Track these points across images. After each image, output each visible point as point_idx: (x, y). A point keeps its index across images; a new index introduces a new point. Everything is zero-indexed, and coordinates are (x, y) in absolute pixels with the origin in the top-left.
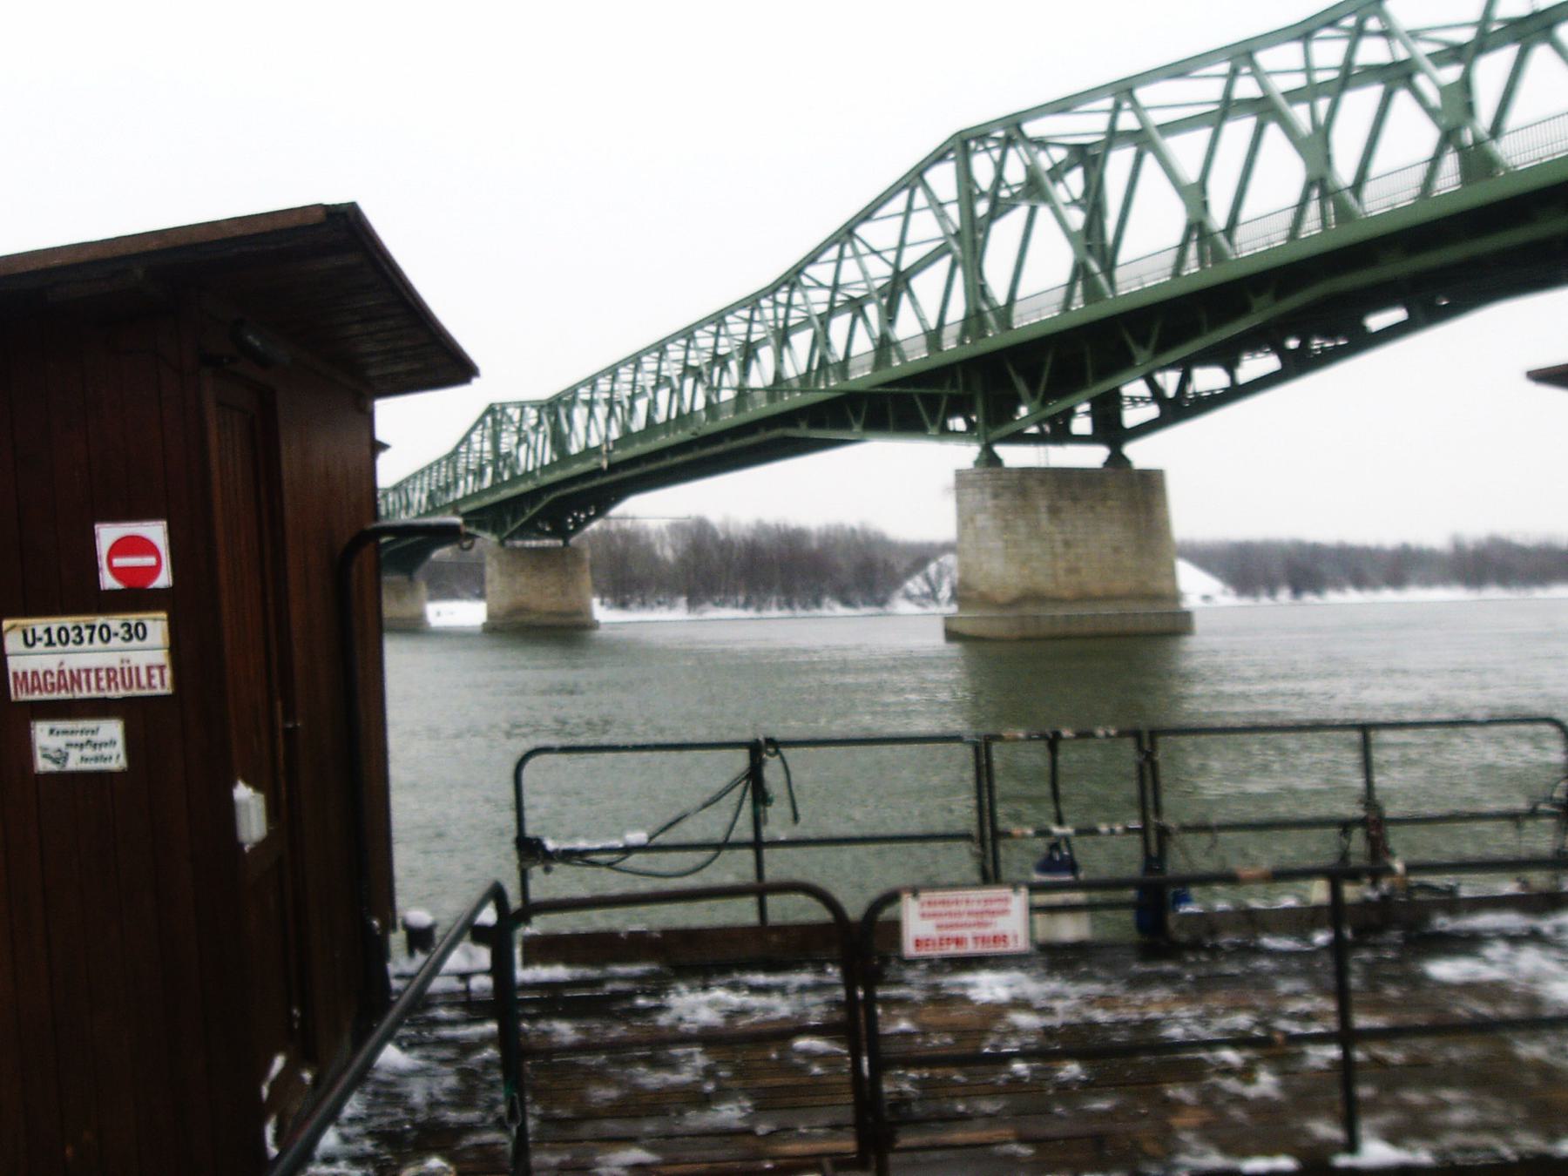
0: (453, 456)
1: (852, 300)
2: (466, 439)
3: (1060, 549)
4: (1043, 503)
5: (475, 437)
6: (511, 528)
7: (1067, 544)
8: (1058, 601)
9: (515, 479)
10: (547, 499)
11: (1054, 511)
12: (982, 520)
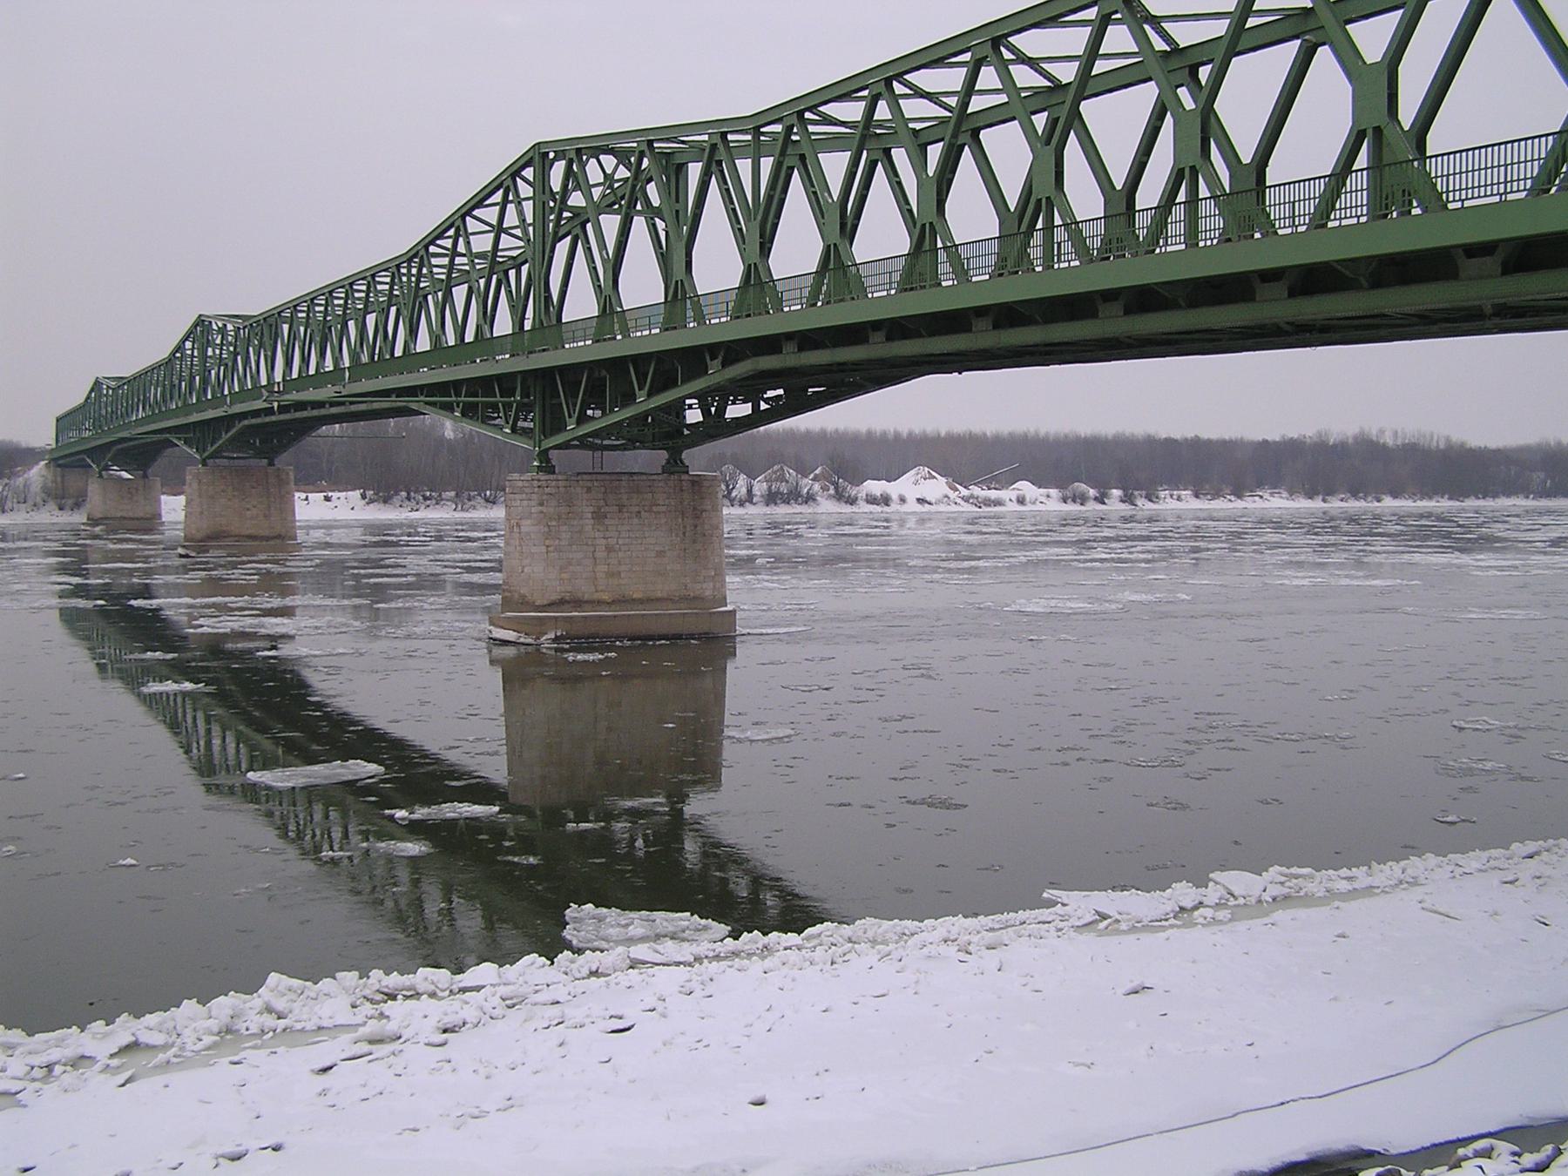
0: (420, 254)
1: (1176, 51)
2: (180, 348)
3: (601, 554)
4: (588, 511)
5: (188, 345)
6: (211, 449)
7: (609, 549)
8: (599, 603)
9: (385, 363)
10: (238, 426)
11: (599, 516)
12: (527, 526)
